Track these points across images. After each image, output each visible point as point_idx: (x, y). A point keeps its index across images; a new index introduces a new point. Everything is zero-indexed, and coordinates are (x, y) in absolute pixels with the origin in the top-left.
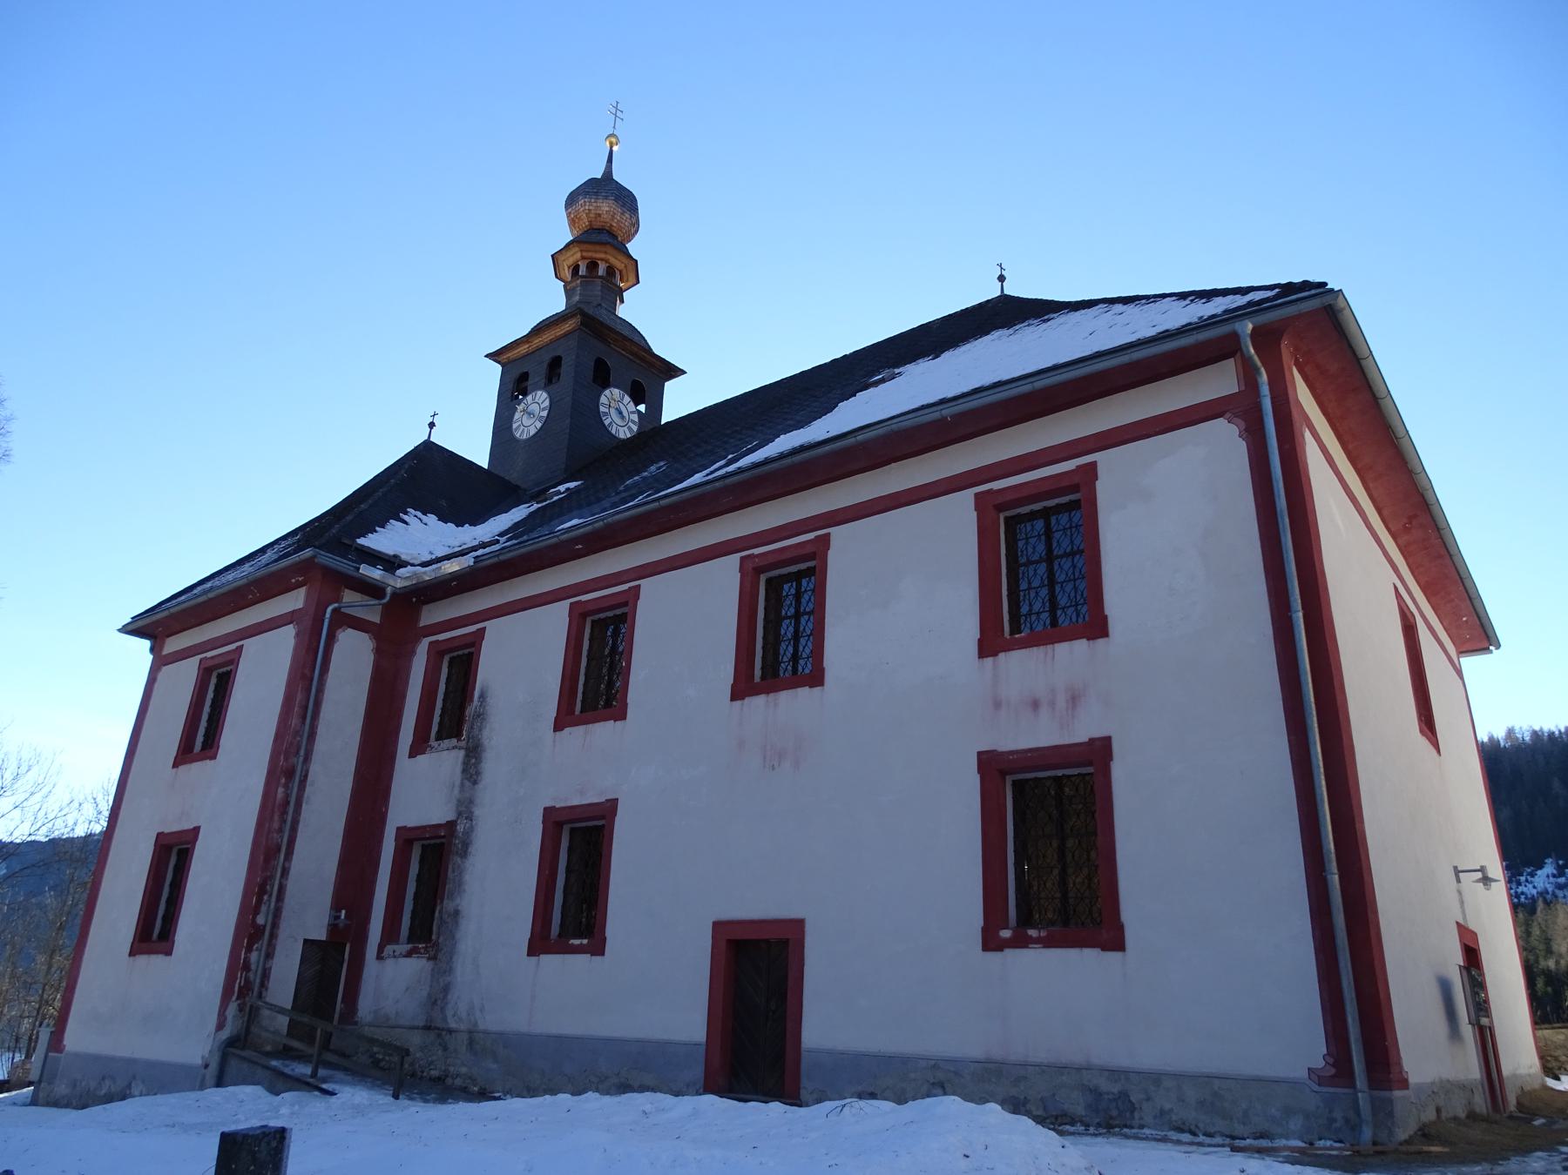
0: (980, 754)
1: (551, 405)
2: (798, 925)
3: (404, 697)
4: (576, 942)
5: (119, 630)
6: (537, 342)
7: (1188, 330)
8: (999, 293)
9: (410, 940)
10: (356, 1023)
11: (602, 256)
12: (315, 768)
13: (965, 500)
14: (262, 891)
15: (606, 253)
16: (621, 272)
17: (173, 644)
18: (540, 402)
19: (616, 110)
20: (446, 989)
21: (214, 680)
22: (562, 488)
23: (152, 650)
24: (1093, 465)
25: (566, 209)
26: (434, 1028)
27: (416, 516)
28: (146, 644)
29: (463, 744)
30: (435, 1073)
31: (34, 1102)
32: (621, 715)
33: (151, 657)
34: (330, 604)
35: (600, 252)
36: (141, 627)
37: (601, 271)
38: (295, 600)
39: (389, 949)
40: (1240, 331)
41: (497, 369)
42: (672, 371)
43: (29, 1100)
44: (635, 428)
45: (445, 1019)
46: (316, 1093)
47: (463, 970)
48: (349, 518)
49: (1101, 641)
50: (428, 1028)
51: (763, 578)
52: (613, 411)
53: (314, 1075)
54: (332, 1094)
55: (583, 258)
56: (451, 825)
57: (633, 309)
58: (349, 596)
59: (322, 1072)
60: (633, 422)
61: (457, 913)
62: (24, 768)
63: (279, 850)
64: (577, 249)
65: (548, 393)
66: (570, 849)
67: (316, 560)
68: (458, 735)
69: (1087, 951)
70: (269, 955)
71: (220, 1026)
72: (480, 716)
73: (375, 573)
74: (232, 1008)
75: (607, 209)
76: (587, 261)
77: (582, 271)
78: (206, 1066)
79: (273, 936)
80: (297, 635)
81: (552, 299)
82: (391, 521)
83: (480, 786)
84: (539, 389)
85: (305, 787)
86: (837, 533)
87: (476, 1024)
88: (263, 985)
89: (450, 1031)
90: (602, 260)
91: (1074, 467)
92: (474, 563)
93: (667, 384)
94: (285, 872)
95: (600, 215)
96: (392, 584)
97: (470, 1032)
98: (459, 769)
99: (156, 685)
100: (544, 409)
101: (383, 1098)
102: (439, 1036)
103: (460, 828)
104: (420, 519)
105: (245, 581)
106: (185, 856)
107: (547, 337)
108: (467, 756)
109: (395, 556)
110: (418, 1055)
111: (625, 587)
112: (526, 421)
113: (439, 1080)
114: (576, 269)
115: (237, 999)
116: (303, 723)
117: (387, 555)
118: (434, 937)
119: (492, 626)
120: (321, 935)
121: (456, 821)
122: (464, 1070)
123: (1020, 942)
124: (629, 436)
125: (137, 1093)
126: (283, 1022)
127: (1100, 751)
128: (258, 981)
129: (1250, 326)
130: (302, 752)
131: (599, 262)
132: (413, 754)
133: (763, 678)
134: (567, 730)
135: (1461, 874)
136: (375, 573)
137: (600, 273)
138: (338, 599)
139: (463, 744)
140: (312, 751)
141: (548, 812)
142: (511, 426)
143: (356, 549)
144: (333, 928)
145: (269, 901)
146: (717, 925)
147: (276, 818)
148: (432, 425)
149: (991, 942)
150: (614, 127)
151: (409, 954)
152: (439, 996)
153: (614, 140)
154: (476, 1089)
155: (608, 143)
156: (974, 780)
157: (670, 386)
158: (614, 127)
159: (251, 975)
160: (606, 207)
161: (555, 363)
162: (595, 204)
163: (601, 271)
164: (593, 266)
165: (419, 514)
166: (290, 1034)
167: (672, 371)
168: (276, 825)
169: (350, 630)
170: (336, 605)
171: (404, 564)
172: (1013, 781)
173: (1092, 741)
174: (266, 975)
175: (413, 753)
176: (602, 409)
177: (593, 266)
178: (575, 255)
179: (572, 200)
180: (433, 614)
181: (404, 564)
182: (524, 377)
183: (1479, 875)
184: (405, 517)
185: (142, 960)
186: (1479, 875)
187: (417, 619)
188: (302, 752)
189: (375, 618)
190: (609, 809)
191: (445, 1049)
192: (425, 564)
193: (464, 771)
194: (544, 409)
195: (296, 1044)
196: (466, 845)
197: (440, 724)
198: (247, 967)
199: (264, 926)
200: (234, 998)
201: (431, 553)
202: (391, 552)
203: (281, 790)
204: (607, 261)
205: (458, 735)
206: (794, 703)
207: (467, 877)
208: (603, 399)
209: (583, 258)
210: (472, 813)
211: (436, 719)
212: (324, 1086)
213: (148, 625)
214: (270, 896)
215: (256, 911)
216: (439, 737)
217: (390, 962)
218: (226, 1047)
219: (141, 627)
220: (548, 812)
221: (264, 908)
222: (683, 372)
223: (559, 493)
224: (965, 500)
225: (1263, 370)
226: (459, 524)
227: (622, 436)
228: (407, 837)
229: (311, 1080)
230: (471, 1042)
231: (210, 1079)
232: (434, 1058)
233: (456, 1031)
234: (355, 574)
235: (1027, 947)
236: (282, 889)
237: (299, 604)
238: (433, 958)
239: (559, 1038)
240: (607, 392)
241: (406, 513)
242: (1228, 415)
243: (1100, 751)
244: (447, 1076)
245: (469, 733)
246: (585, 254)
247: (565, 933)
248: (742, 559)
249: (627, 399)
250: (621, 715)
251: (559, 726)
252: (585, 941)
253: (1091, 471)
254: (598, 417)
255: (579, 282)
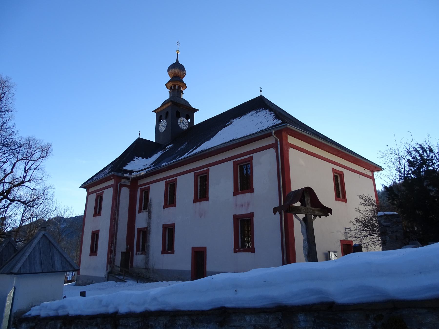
0: (233, 215)
1: (167, 124)
2: (205, 248)
3: (136, 200)
4: (170, 251)
5: (80, 187)
6: (163, 108)
7: (266, 131)
8: (260, 95)
9: (142, 251)
10: (133, 268)
11: (177, 84)
12: (120, 217)
13: (231, 163)
14: (112, 243)
15: (178, 83)
16: (182, 86)
17: (91, 190)
18: (165, 123)
19: (178, 43)
20: (148, 261)
21: (99, 198)
22: (168, 147)
23: (87, 191)
24: (252, 156)
25: (168, 72)
26: (147, 269)
27: (136, 158)
28: (85, 189)
29: (148, 211)
30: (147, 277)
31: (76, 285)
32: (175, 206)
33: (87, 192)
34: (119, 183)
35: (176, 83)
36: (83, 186)
37: (177, 87)
38: (112, 182)
39: (138, 253)
40: (272, 132)
41: (155, 114)
42: (196, 110)
43: (75, 284)
44: (187, 126)
45: (148, 267)
46: (124, 282)
47: (151, 257)
48: (121, 163)
49: (253, 193)
50: (145, 268)
51: (199, 177)
52: (182, 123)
53: (124, 278)
54: (126, 282)
55: (172, 85)
56: (147, 228)
57: (186, 95)
58: (123, 181)
59: (125, 278)
60: (187, 125)
61: (149, 246)
62: (66, 211)
63: (114, 234)
64: (171, 83)
65: (166, 121)
66: (168, 233)
67: (115, 174)
68: (147, 209)
69: (249, 253)
70: (115, 255)
71: (107, 270)
72: (150, 205)
73: (128, 175)
74: (109, 266)
75: (177, 71)
76: (173, 85)
77: (172, 88)
78: (105, 277)
79: (115, 252)
80: (113, 190)
81: (166, 95)
82: (131, 161)
83: (151, 220)
84: (164, 120)
85: (118, 221)
86: (211, 168)
87: (154, 268)
88: (114, 261)
89: (149, 269)
90: (177, 84)
91: (249, 157)
92: (146, 173)
93: (195, 113)
94: (116, 239)
95: (175, 73)
96: (131, 177)
97: (153, 269)
98: (147, 216)
99: (88, 199)
100: (165, 125)
101: (135, 283)
102: (148, 270)
103: (148, 228)
104: (138, 159)
105: (102, 178)
106: (98, 235)
107: (165, 107)
108: (148, 213)
109: (132, 170)
110: (144, 274)
111: (174, 178)
112: (162, 128)
113: (148, 278)
114: (171, 87)
115: (109, 264)
116: (116, 208)
117: (130, 170)
118: (145, 250)
119: (152, 185)
120: (125, 251)
121: (147, 227)
122: (152, 276)
123: (239, 251)
124: (186, 128)
125: (94, 283)
126: (119, 269)
127: (252, 215)
128: (113, 260)
129: (274, 132)
130: (117, 214)
131: (176, 85)
132: (139, 213)
133: (200, 198)
134: (166, 208)
135: (346, 229)
136: (128, 175)
137: (177, 88)
138: (120, 181)
139: (148, 211)
140: (119, 214)
141: (163, 225)
142: (159, 129)
143: (123, 170)
144: (127, 249)
145: (113, 244)
146: (193, 248)
147: (113, 228)
148: (139, 134)
149: (235, 251)
150: (178, 48)
151: (141, 254)
152: (147, 262)
153: (178, 52)
154: (154, 280)
155: (177, 52)
156: (232, 220)
157: (196, 114)
158: (178, 48)
159: (112, 260)
160: (177, 71)
161: (167, 113)
162: (174, 71)
163: (177, 87)
164: (175, 86)
165: (137, 157)
166: (120, 271)
167: (196, 110)
168: (113, 230)
169: (124, 187)
170: (120, 183)
171: (133, 172)
172: (241, 220)
173: (251, 213)
174: (114, 259)
175: (139, 212)
176: (179, 123)
177: (175, 86)
178: (170, 84)
179: (169, 70)
180: (141, 182)
181: (133, 172)
182: (161, 116)
183: (349, 229)
184: (134, 159)
185: (92, 256)
186: (349, 229)
187: (137, 183)
188: (117, 214)
189: (129, 184)
190: (174, 225)
191: (149, 272)
192: (138, 172)
193: (148, 216)
194: (165, 125)
195: (120, 273)
196: (150, 232)
197: (144, 206)
198: (110, 258)
199: (113, 250)
200: (109, 264)
201: (139, 168)
202: (130, 169)
203: (113, 222)
204: (178, 85)
205: (147, 209)
206: (204, 203)
207: (150, 238)
208: (179, 121)
209: (172, 85)
210: (150, 225)
211: (143, 205)
212: (125, 281)
213: (86, 186)
214: (114, 243)
215: (111, 247)
216: (144, 209)
217: (138, 256)
218: (108, 273)
219: (83, 186)
220: (163, 225)
221: (113, 246)
222: (199, 110)
223: (168, 148)
224: (231, 163)
225: (278, 139)
226: (147, 158)
227: (184, 129)
228: (139, 230)
229: (123, 280)
230: (153, 271)
231: (106, 280)
232: (147, 274)
233: (151, 269)
234: (123, 176)
235: (240, 252)
236: (116, 242)
237: (113, 183)
238: (145, 255)
239: (168, 270)
240: (180, 119)
241: (134, 158)
242: (274, 147)
243: (252, 215)
244: (149, 277)
245: (148, 209)
246: (173, 84)
247: (168, 250)
248: (194, 173)
249: (185, 119)
250: (175, 206)
251: (164, 208)
252: (171, 251)
253: (251, 158)
254: (178, 125)
255: (172, 91)
